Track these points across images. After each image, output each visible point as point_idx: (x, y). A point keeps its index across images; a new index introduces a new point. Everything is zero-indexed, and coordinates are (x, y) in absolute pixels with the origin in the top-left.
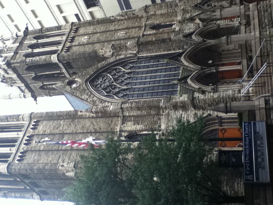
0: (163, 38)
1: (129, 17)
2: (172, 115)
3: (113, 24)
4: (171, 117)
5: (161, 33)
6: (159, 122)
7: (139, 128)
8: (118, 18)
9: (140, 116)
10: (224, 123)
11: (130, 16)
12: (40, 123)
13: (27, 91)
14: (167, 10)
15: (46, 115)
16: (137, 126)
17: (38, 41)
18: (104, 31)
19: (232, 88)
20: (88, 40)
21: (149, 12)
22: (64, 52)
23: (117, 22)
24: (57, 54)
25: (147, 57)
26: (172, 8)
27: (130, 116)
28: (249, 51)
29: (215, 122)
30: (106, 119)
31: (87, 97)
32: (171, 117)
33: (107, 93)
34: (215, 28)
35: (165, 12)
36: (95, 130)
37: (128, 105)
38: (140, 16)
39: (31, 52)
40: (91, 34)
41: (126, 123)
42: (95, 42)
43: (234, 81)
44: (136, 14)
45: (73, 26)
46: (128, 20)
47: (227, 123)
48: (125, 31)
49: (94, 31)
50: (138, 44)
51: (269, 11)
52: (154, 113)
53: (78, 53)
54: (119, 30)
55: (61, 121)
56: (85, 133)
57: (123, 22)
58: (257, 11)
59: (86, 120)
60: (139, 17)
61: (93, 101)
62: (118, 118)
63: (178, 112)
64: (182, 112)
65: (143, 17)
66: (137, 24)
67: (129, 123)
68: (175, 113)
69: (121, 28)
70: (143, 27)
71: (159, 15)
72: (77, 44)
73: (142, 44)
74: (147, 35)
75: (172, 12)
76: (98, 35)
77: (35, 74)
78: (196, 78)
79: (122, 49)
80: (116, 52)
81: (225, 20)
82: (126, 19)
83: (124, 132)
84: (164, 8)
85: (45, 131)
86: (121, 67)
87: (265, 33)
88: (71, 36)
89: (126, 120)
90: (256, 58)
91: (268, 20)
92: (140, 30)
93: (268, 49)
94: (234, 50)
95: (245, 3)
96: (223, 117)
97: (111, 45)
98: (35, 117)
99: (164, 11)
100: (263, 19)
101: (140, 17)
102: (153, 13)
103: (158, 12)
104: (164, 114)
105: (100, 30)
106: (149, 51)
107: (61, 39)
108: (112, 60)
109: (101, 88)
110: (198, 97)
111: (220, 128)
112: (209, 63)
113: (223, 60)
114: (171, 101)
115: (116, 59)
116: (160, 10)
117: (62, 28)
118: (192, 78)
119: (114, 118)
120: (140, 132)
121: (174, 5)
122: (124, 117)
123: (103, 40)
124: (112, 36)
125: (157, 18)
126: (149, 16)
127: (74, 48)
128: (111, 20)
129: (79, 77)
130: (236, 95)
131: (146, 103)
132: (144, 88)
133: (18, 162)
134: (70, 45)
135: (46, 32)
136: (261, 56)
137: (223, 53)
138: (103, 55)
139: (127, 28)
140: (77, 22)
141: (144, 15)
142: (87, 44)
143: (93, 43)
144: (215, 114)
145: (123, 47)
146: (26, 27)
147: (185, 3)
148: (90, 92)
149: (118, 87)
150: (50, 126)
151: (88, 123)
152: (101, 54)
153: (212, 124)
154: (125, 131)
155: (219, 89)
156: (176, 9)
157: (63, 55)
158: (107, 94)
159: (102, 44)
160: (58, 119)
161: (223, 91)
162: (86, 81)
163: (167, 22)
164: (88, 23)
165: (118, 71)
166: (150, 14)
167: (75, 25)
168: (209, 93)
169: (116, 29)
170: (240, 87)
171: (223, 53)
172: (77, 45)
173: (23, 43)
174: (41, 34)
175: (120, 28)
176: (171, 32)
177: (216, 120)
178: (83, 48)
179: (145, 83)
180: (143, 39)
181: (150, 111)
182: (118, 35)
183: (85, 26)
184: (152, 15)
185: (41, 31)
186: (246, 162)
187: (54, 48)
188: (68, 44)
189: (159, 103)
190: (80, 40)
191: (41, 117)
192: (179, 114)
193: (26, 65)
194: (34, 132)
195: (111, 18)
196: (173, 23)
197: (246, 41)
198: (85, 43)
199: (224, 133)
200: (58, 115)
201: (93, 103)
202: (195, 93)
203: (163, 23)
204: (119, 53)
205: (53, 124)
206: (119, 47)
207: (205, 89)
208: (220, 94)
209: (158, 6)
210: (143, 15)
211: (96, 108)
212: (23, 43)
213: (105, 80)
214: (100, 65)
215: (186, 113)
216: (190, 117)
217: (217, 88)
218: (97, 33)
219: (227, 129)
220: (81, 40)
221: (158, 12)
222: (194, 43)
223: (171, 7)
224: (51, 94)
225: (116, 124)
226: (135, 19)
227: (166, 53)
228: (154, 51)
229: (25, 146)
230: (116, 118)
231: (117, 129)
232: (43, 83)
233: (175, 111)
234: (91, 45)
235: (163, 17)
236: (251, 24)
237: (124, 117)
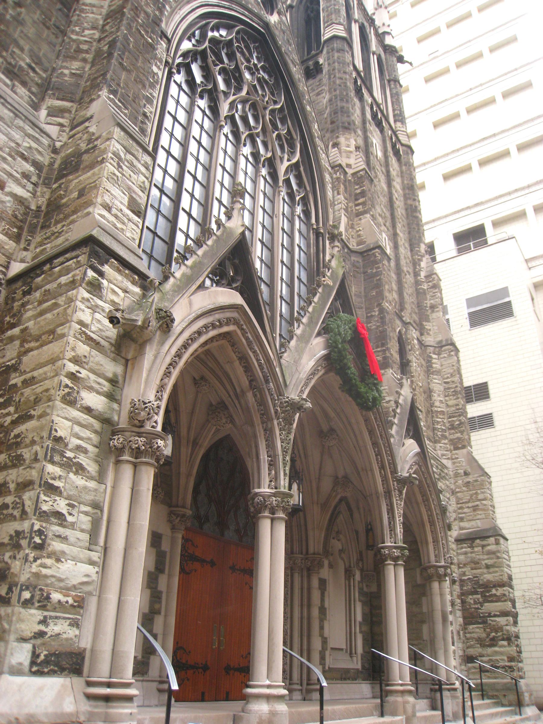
1: (425, 294)
11: (428, 297)
14: (442, 412)
17: (373, 55)
19: (112, 597)
21: (439, 354)
26: (449, 429)
35: (437, 404)
43: (159, 621)
46: (416, 290)
50: (374, 249)
52: (66, 72)
60: (424, 323)
63: (26, 176)
71: (429, 383)
79: (356, 200)
84: (450, 403)
99: (441, 401)
102: (436, 366)
103: (436, 381)
116: (445, 389)
121: (459, 435)
126: (428, 351)
130: (29, 620)
135: (390, 90)
146: (405, 59)
147: (466, 474)
155: (127, 471)
156: (443, 441)
161: (97, 506)
166: (434, 356)
168: (113, 382)
170: (103, 672)
186: (468, 635)
202: (137, 290)
207: (149, 353)
208: (80, 469)
210: (428, 334)
217: (137, 453)
221: (436, 381)
223: (452, 427)
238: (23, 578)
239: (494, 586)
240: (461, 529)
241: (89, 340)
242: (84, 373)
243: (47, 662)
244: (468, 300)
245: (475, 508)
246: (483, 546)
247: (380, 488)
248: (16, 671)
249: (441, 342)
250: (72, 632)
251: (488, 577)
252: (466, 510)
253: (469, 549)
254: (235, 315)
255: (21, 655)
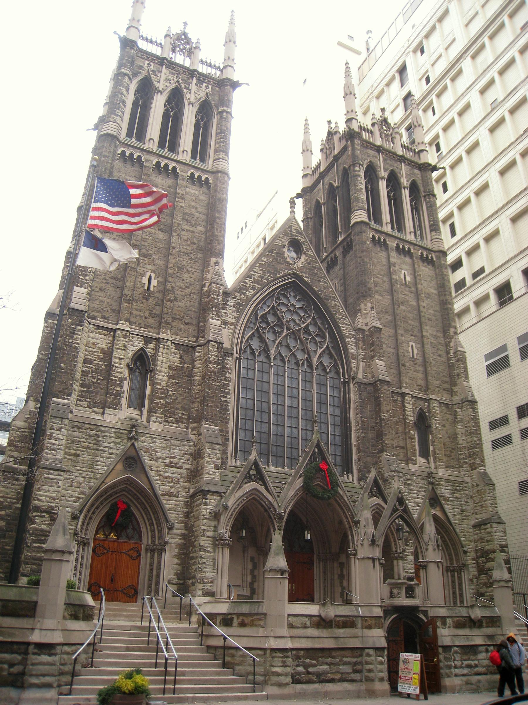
0: (386, 435)
2: (182, 448)
3: (440, 334)
4: (176, 446)
5: (405, 434)
6: (169, 419)
7: (161, 377)
8: (452, 344)
9: (191, 380)
10: (152, 558)
12: (205, 189)
13: (317, 176)
15: (219, 199)
16: (165, 373)
18: (422, 314)
20: (402, 282)
22: (373, 236)
23: (443, 342)
24: (367, 220)
25: (346, 400)
27: (193, 360)
28: (243, 620)
29: (155, 537)
30: (195, 312)
31: (256, 276)
32: (176, 446)
33: (264, 317)
34: (394, 549)
35: (461, 442)
36: (168, 290)
37: (215, 356)
38: (455, 389)
39: (380, 176)
40: (417, 288)
41: (178, 351)
42: (395, 294)
44: (459, 381)
45: (437, 254)
47: (151, 564)
48: (418, 357)
49: (423, 295)
51: (357, 676)
53: (367, 260)
54: (423, 346)
55: (204, 226)
56: (167, 271)
57: (443, 353)
58: (360, 646)
59: (197, 274)
61: (245, 288)
62: (194, 337)
63: (188, 460)
64: (188, 469)
65: (452, 396)
66: (434, 382)
67: (176, 359)
68: (186, 454)
69: (425, 349)
70: (427, 395)
72: (392, 260)
73: (377, 390)
74: (403, 402)
75: (459, 459)
76: (414, 303)
77: (338, 187)
78: (256, 500)
80: (364, 337)
81: (413, 573)
82: (449, 359)
83: (156, 347)
85: (182, 198)
86: (328, 346)
87: (278, 661)
88: (414, 249)
89: (185, 353)
90: (222, 635)
91: (325, 673)
92: (420, 390)
93: (240, 667)
94: (340, 590)
95: (393, 617)
96: (163, 554)
97: (380, 326)
98: (217, 179)
99: (463, 440)
100: (329, 660)
101: (452, 389)
104: (190, 430)
105: (424, 307)
106: (361, 405)
107: (408, 231)
108: (346, 329)
109: (279, 305)
110: (206, 504)
111: (143, 547)
112: (306, 532)
113: (321, 563)
114: (207, 445)
115: (349, 337)
117: (433, 233)
118: (257, 493)
119: (196, 328)
120: (150, 380)
122: (194, 348)
123: (398, 312)
124: (407, 331)
125: (448, 426)
127: (383, 254)
128: (449, 330)
129: (309, 263)
130: (201, 586)
131: (212, 393)
132: (268, 393)
133: (119, 152)
134: (389, 246)
135: (426, 203)
136: (226, 648)
137: (336, 565)
138: (360, 310)
139: (425, 363)
140: (446, 261)
141: (457, 399)
142: (391, 279)
143: (392, 291)
144: (172, 538)
145: (373, 350)
147: (477, 485)
148: (269, 283)
149: (276, 340)
150: (193, 207)
151: (190, 277)
152: (362, 306)
153: (151, 531)
154: (157, 349)
155: (221, 550)
157: (364, 232)
158: (259, 317)
159: (390, 310)
160: (207, 222)
161: (214, 559)
162: (295, 275)
163: (434, 446)
164: (444, 284)
165: (318, 339)
167: (438, 258)
168: (215, 527)
169: (425, 339)
171: (336, 565)
172: (389, 261)
173: (401, 163)
174: (422, 194)
175: (427, 346)
176: (407, 453)
177: (159, 539)
178: (382, 273)
179: (279, 395)
180: (388, 392)
181: (198, 402)
182: (411, 343)
183: (436, 278)
184: (455, 415)
185: (429, 195)
187: (386, 217)
188: (392, 244)
189: (211, 419)
190: (404, 266)
191: (216, 191)
192: (183, 463)
193: (350, 167)
194: (183, 179)
195: (452, 330)
196: (432, 459)
197: (265, 614)
198: (394, 276)
199: (128, 555)
200: (214, 221)
201: (240, 288)
203: (433, 437)
204: (361, 343)
205: (198, 212)
206: (373, 342)
208: (208, 551)
209: (473, 426)
210: (456, 395)
211: (219, 292)
212: (401, 163)
213: (296, 312)
214: (335, 304)
215: (181, 478)
216: (172, 484)
217: (222, 545)
218: (418, 298)
219: (137, 561)
220: (402, 269)
222: (357, 501)
224: (305, 223)
225: (180, 333)
226: (448, 380)
227: (354, 443)
228: (359, 416)
229: (154, 163)
230: (195, 333)
231: (165, 333)
232: (324, 204)
233: (191, 454)
234: (387, 288)
235: (449, 438)
236: (320, 630)
237: (194, 348)
238: (198, 578)
239: (491, 553)
240: (476, 519)
241: (206, 519)
242: (206, 528)
243: (205, 594)
244: (519, 338)
245: (482, 506)
246: (485, 529)
247: (347, 526)
248: (199, 596)
249: (462, 399)
250: (211, 588)
251: (488, 547)
252: (478, 508)
253: (479, 532)
254: (254, 491)
255: (200, 593)
